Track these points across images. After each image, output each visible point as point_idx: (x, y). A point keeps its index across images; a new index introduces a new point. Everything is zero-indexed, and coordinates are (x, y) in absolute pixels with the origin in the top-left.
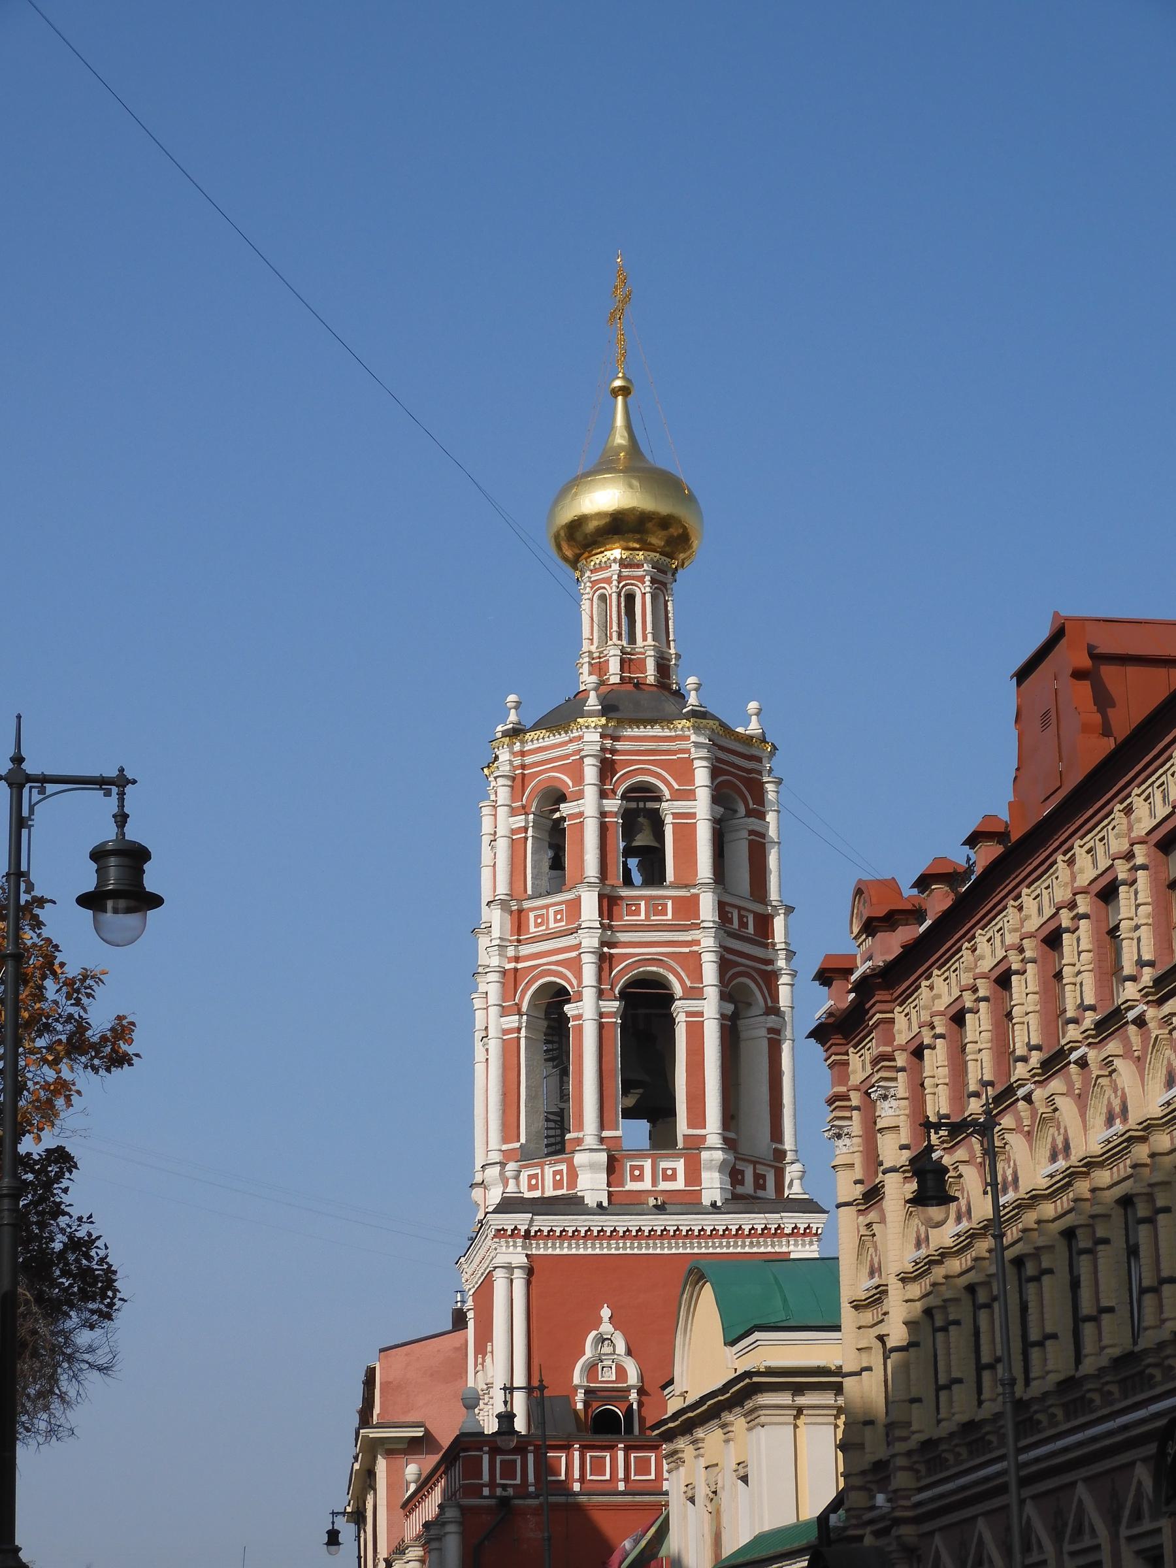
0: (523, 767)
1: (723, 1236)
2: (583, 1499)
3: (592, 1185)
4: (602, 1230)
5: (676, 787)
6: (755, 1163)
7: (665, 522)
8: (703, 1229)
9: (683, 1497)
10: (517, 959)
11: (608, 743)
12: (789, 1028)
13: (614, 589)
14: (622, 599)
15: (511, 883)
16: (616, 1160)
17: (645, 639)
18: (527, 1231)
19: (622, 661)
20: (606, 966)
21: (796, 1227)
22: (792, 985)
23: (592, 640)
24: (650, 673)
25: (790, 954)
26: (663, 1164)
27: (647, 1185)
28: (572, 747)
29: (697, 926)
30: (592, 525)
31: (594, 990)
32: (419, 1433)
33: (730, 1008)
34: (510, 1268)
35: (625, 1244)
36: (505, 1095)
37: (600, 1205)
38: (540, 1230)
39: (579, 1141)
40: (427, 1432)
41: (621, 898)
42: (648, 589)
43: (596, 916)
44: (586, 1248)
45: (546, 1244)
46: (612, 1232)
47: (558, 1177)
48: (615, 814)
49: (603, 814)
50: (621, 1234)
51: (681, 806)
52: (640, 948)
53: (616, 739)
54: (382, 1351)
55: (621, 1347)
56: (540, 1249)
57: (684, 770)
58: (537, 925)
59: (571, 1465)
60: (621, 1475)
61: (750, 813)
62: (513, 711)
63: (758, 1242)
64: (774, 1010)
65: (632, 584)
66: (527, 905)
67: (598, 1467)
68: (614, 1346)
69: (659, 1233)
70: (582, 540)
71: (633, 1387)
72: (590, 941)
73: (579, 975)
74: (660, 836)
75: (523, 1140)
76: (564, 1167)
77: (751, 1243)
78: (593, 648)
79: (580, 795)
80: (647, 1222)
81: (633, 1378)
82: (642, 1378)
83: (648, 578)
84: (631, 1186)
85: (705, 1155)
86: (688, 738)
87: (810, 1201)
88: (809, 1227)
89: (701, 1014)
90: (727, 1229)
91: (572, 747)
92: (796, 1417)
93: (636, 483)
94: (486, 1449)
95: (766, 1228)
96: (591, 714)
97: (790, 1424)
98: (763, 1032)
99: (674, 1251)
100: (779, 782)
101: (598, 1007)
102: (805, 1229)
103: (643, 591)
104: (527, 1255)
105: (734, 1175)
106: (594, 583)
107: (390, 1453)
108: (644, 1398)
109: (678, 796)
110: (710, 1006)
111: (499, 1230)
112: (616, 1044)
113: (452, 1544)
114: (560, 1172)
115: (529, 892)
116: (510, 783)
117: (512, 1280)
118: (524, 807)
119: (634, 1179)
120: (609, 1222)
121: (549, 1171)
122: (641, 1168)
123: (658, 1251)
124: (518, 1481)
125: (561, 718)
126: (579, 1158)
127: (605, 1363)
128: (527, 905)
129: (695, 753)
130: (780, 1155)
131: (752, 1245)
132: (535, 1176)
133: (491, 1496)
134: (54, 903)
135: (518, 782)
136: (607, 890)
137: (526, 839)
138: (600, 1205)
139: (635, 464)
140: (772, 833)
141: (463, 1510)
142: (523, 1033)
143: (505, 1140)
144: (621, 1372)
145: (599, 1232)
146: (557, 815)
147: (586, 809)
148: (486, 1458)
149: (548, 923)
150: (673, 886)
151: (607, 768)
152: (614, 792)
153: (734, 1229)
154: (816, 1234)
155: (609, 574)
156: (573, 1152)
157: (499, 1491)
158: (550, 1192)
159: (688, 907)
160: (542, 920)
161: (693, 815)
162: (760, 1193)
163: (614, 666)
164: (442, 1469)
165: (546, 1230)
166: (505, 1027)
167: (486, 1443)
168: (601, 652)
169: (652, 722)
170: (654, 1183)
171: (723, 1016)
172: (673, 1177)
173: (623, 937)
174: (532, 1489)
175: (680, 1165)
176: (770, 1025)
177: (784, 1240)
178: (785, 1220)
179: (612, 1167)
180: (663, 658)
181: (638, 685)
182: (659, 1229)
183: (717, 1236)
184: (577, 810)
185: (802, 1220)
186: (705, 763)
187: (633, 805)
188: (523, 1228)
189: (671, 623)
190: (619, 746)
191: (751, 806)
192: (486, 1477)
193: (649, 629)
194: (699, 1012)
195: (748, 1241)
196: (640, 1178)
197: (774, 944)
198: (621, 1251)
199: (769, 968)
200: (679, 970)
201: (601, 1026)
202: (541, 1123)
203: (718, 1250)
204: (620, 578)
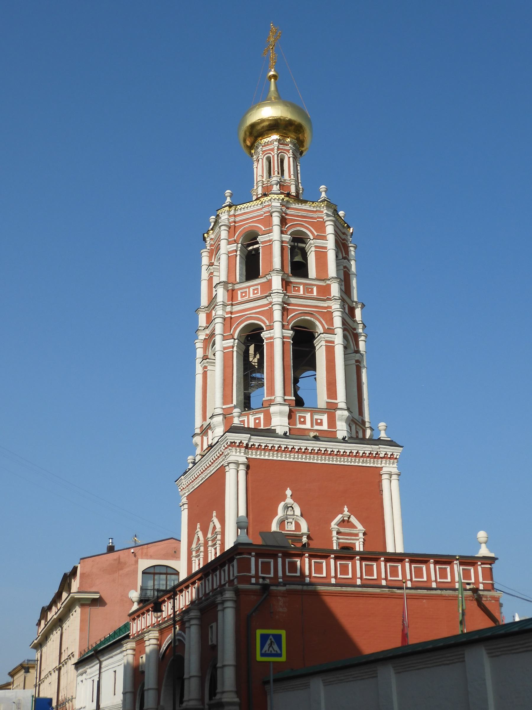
1: (349, 456)
3: (280, 422)
11: (284, 208)
13: (276, 153)
17: (290, 177)
18: (247, 445)
20: (285, 313)
22: (365, 341)
25: (365, 326)
26: (316, 417)
27: (308, 426)
29: (330, 299)
30: (266, 123)
31: (280, 323)
32: (97, 596)
34: (237, 464)
36: (224, 380)
38: (253, 445)
41: (291, 282)
42: (291, 155)
43: (280, 288)
44: (277, 457)
45: (256, 453)
47: (257, 421)
48: (287, 243)
51: (319, 242)
52: (303, 304)
53: (288, 208)
54: (81, 559)
56: (254, 455)
57: (320, 226)
58: (242, 297)
60: (333, 574)
63: (366, 461)
64: (357, 351)
66: (237, 287)
68: (294, 511)
70: (257, 132)
72: (277, 299)
76: (262, 416)
77: (363, 461)
78: (264, 180)
80: (312, 445)
81: (304, 528)
83: (291, 151)
84: (299, 426)
86: (322, 212)
87: (391, 441)
89: (333, 342)
94: (253, 554)
98: (354, 362)
100: (355, 248)
101: (282, 333)
104: (247, 458)
107: (82, 605)
108: (310, 542)
111: (231, 443)
112: (290, 353)
114: (259, 419)
115: (238, 280)
117: (238, 471)
118: (235, 241)
119: (301, 423)
121: (252, 418)
122: (304, 417)
128: (237, 287)
130: (364, 423)
133: (257, 584)
135: (232, 229)
136: (285, 277)
137: (236, 256)
138: (285, 434)
140: (353, 269)
141: (238, 592)
143: (224, 404)
144: (298, 526)
148: (253, 560)
151: (283, 221)
154: (396, 458)
155: (273, 147)
156: (270, 406)
157: (261, 581)
159: (325, 291)
164: (199, 576)
165: (257, 444)
167: (253, 550)
170: (312, 425)
172: (321, 424)
175: (325, 418)
176: (356, 359)
177: (380, 460)
178: (381, 449)
179: (291, 416)
184: (268, 239)
186: (332, 223)
188: (245, 442)
192: (253, 572)
193: (292, 172)
194: (329, 343)
195: (361, 459)
196: (304, 423)
198: (296, 460)
200: (322, 320)
201: (283, 343)
203: (346, 463)
204: (278, 149)
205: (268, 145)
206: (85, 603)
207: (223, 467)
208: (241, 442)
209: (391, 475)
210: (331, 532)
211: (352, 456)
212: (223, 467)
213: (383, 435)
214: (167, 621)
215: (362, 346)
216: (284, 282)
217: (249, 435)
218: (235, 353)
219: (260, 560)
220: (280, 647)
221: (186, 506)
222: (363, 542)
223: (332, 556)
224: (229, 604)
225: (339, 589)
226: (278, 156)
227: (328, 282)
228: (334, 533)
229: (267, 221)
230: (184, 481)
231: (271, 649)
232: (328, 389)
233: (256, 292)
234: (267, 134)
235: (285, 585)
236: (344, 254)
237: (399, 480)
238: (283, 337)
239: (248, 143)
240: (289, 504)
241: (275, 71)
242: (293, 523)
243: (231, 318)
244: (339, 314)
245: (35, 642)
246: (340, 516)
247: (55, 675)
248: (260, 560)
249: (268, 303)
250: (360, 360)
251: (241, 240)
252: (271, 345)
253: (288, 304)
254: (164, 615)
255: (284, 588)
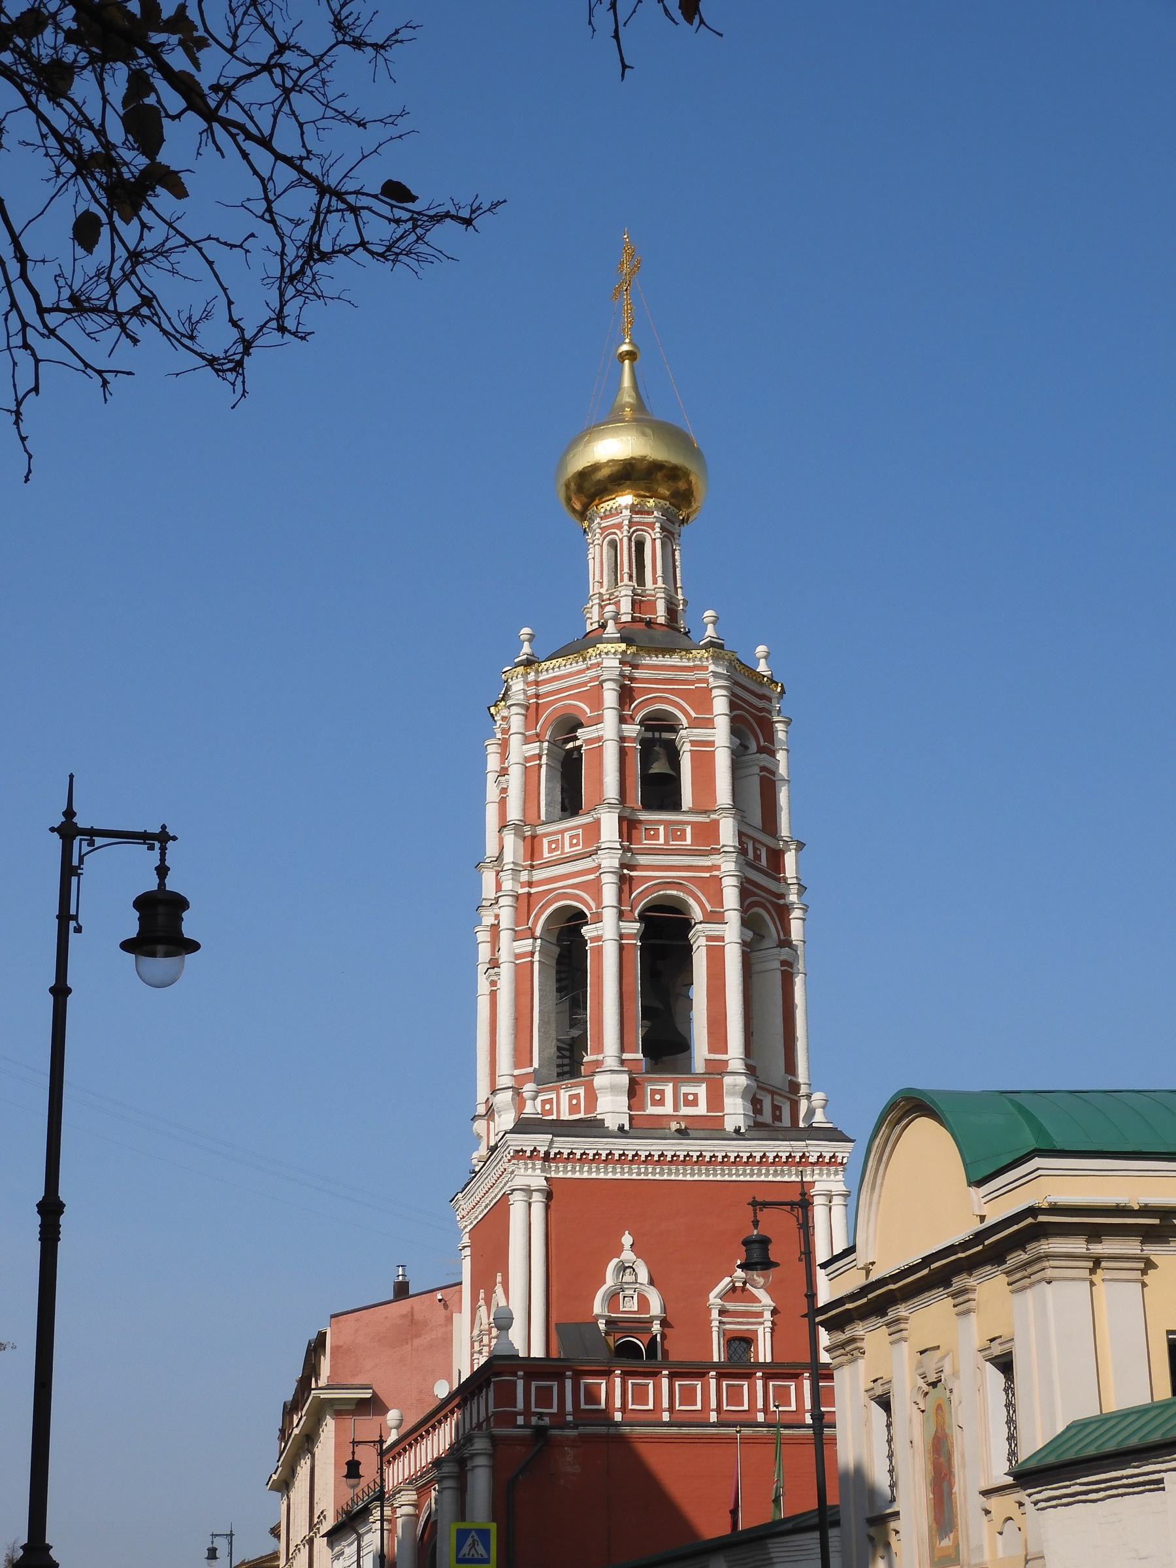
0: (537, 696)
1: (747, 1163)
2: (626, 1430)
3: (612, 1107)
4: (624, 1154)
5: (694, 715)
6: (773, 1093)
7: (673, 473)
8: (726, 1156)
9: (864, 1398)
10: (530, 884)
11: (627, 670)
12: (801, 962)
13: (625, 533)
14: (633, 544)
15: (524, 810)
16: (637, 1083)
17: (655, 582)
18: (547, 1153)
19: (633, 602)
20: (626, 887)
21: (821, 1156)
22: (804, 920)
23: (601, 583)
24: (661, 615)
25: (802, 889)
27: (668, 1109)
28: (591, 673)
29: (716, 851)
30: (605, 472)
31: (615, 910)
32: (367, 1394)
33: (750, 935)
34: (528, 1191)
35: (646, 1169)
37: (621, 1128)
38: (559, 1153)
39: (598, 1063)
40: (375, 1394)
41: (640, 822)
42: (658, 535)
43: (616, 837)
44: (606, 1172)
45: (565, 1167)
46: (634, 1156)
47: (574, 1102)
48: (633, 740)
49: (622, 739)
50: (643, 1158)
51: (699, 733)
52: (664, 866)
53: (635, 667)
54: (333, 1316)
55: (643, 1275)
56: (560, 1172)
57: (702, 699)
58: (551, 850)
59: (613, 1392)
60: (665, 1405)
61: (761, 750)
62: (526, 643)
63: (782, 1171)
64: (786, 943)
65: (642, 530)
66: (540, 830)
67: (641, 1397)
68: (636, 1275)
69: (682, 1158)
70: (592, 488)
71: (656, 1317)
72: (609, 861)
73: (598, 896)
74: (675, 764)
75: (536, 1064)
77: (776, 1171)
78: (603, 591)
79: (599, 720)
80: (670, 1147)
81: (656, 1308)
82: (664, 1309)
83: (658, 525)
84: (651, 1110)
85: (728, 1080)
86: (706, 668)
87: (834, 1130)
88: (834, 1156)
89: (722, 939)
90: (751, 1156)
91: (591, 673)
92: (1092, 1271)
93: (648, 431)
94: (521, 1373)
95: (790, 1156)
96: (610, 641)
97: (1083, 1279)
98: (777, 965)
99: (696, 1178)
100: (788, 723)
102: (831, 1158)
103: (653, 539)
104: (546, 1179)
105: (755, 1104)
106: (603, 529)
107: (338, 1414)
108: (667, 1330)
109: (695, 724)
110: (731, 931)
111: (517, 1152)
113: (480, 1481)
114: (577, 1096)
115: (543, 818)
116: (523, 712)
118: (537, 735)
119: (655, 1103)
120: (631, 1146)
121: (564, 1096)
122: (662, 1092)
123: (681, 1177)
124: (555, 1410)
125: (581, 645)
126: (599, 1081)
127: (627, 1292)
128: (540, 830)
129: (713, 682)
130: (795, 1087)
131: (775, 1173)
132: (550, 1101)
134: (223, 156)
135: (532, 711)
136: (627, 813)
137: (540, 766)
138: (621, 1128)
139: (644, 418)
140: (782, 770)
141: (494, 1440)
142: (537, 957)
143: (517, 1065)
144: (643, 1302)
145: (620, 1155)
146: (570, 745)
147: (606, 736)
148: (520, 1384)
149: (563, 848)
150: (691, 811)
151: (626, 695)
152: (632, 718)
153: (758, 1155)
154: (841, 1164)
156: (593, 1074)
158: (565, 1116)
159: (707, 834)
160: (556, 845)
161: (711, 744)
162: (778, 1124)
163: (626, 606)
166: (517, 951)
167: (520, 1367)
168: (611, 594)
169: (670, 651)
170: (676, 1108)
171: (744, 944)
172: (694, 1103)
173: (642, 860)
174: (570, 1418)
175: (702, 1090)
176: (783, 958)
177: (809, 1169)
178: (810, 1149)
179: (633, 1090)
180: (671, 603)
181: (650, 624)
182: (682, 1154)
183: (741, 1164)
184: (595, 735)
185: (827, 1148)
186: (724, 692)
187: (649, 735)
188: (542, 1150)
189: (678, 570)
190: (638, 674)
191: (762, 743)
192: (520, 1405)
193: (659, 572)
194: (719, 936)
195: (772, 1169)
196: (661, 1103)
197: (785, 879)
198: (642, 1177)
199: (782, 902)
200: (700, 894)
201: (621, 948)
202: (553, 1050)
203: (742, 1178)
204: (631, 524)
205: (611, 515)
206: (341, 1409)
207: (505, 1196)
208: (535, 1149)
209: (830, 1197)
210: (708, 1311)
211: (754, 1164)
212: (505, 1196)
213: (819, 1118)
214: (427, 1472)
215: (796, 929)
216: (625, 824)
217: (550, 1136)
218: (536, 966)
219: (534, 1384)
220: (488, 1549)
221: (467, 1251)
222: (772, 1329)
223: (665, 1372)
224: (481, 1461)
225: (674, 1430)
226: (630, 540)
227: (713, 816)
228: (715, 1314)
229: (595, 697)
230: (462, 1202)
231: (473, 1551)
232: (711, 1034)
233: (575, 841)
234: (612, 492)
235: (576, 1427)
236: (762, 740)
237: (846, 1205)
238: (621, 936)
239: (578, 507)
240: (628, 1262)
241: (631, 343)
242: (635, 1297)
243: (529, 894)
244: (733, 881)
245: (275, 1477)
246: (727, 1280)
247: (305, 1551)
248: (534, 1384)
249: (592, 867)
250: (790, 960)
251: (549, 733)
252: (599, 951)
253: (632, 868)
254: (363, 1482)
255: (574, 1432)
